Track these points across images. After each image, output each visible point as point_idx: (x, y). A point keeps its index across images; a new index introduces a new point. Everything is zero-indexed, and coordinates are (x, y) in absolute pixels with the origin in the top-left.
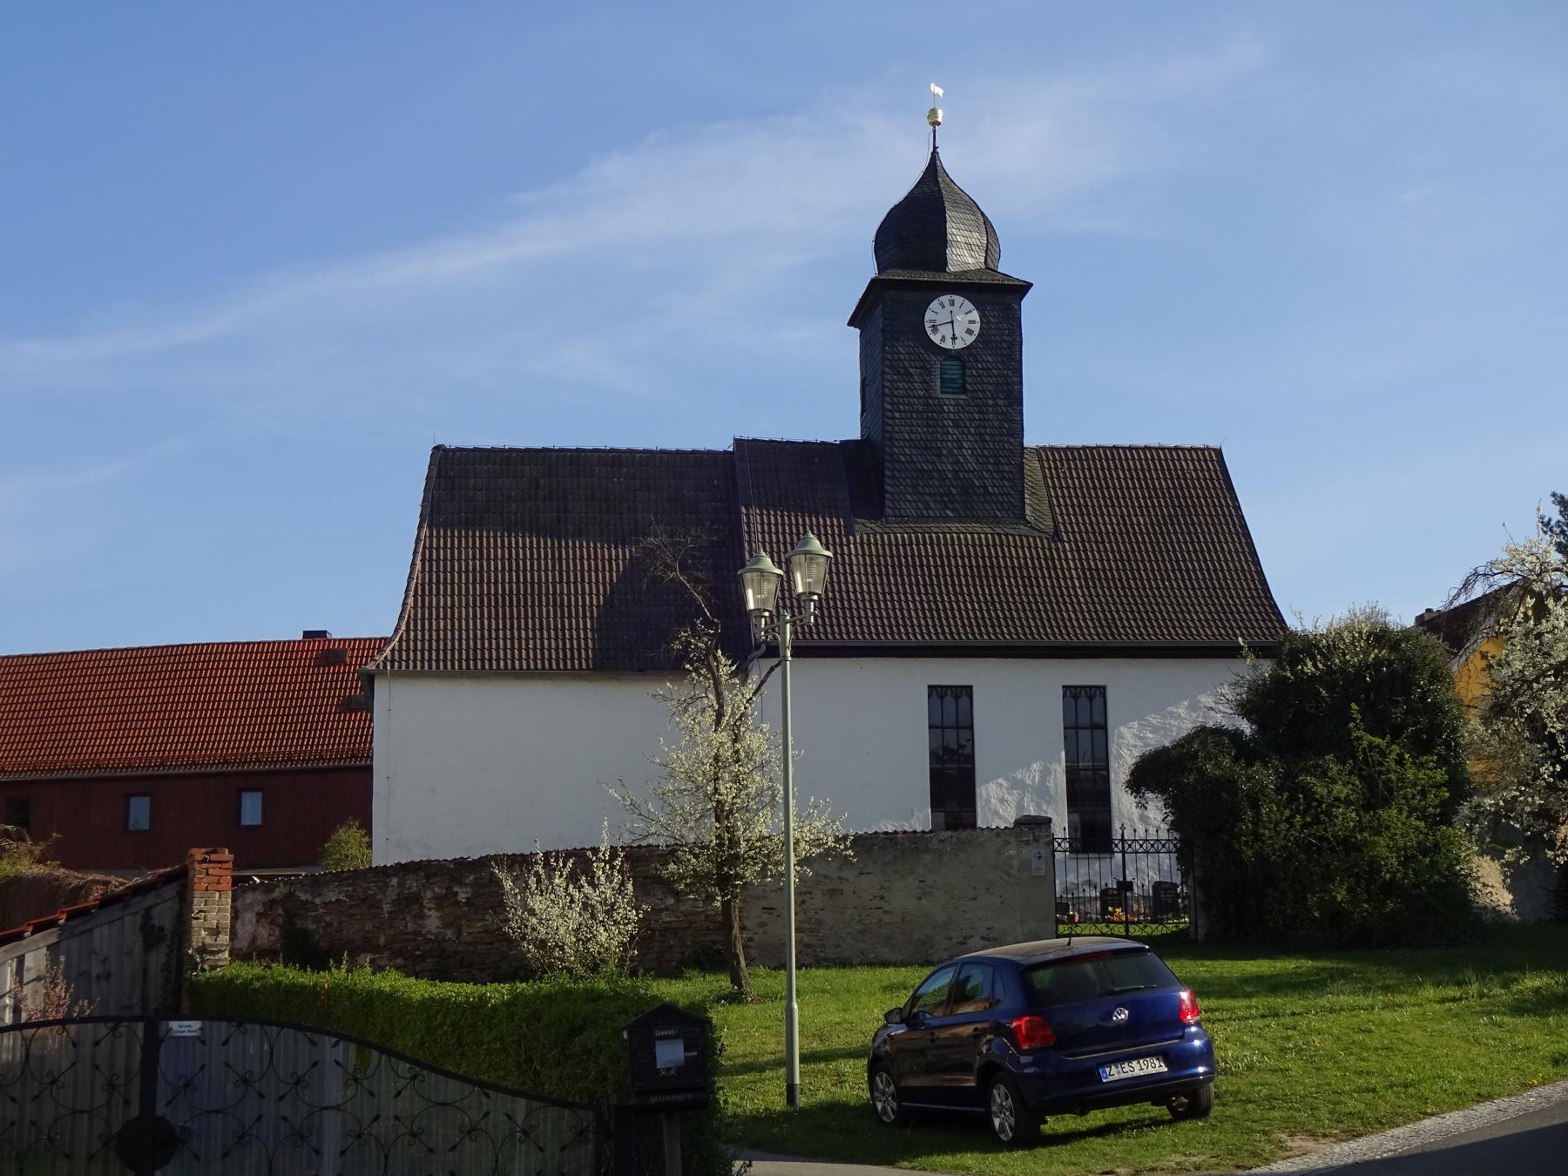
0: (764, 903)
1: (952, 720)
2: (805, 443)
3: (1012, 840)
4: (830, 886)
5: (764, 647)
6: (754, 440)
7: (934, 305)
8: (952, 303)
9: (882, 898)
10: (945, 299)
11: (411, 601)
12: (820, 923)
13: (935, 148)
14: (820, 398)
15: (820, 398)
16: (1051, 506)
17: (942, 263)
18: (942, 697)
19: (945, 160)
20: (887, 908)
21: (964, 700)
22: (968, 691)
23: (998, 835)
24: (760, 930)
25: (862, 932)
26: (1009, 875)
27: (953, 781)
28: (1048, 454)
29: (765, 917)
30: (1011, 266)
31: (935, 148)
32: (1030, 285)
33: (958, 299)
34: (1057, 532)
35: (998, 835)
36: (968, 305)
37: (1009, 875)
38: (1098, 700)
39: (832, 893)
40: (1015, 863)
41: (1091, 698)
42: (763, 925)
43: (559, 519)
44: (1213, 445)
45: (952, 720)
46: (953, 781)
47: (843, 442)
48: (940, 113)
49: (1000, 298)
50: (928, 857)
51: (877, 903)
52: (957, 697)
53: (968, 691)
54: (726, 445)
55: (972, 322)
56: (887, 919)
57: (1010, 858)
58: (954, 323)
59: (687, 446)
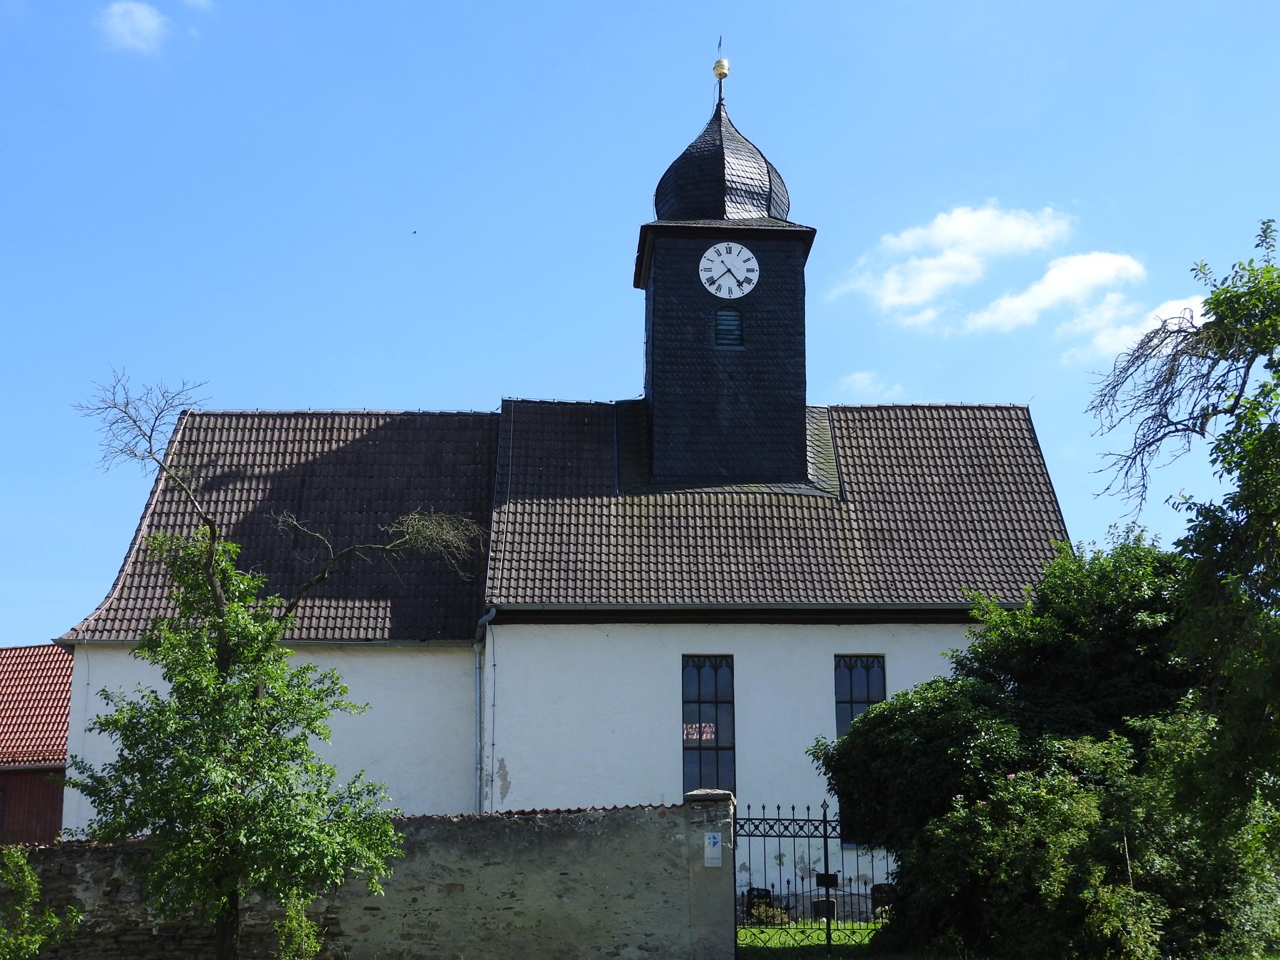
0: (367, 902)
1: (708, 687)
2: (578, 404)
3: (680, 821)
4: (449, 880)
5: (493, 611)
6: (523, 401)
7: (710, 253)
8: (729, 251)
9: (513, 895)
10: (722, 247)
11: (129, 569)
12: (434, 927)
13: (721, 99)
14: (601, 356)
15: (601, 356)
16: (839, 465)
17: (720, 213)
18: (699, 668)
19: (728, 112)
20: (518, 908)
21: (723, 672)
22: (728, 660)
23: (662, 815)
24: (361, 937)
25: (486, 939)
26: (675, 865)
27: (710, 760)
28: (837, 412)
29: (367, 919)
30: (798, 217)
31: (721, 99)
32: (812, 233)
33: (736, 247)
34: (842, 492)
35: (662, 815)
36: (747, 253)
37: (675, 865)
38: (875, 671)
39: (450, 889)
40: (684, 850)
41: (868, 669)
42: (364, 929)
43: (303, 482)
44: (1020, 403)
45: (708, 687)
46: (710, 760)
47: (618, 403)
48: (726, 63)
49: (784, 249)
50: (572, 844)
51: (506, 901)
52: (716, 669)
53: (728, 660)
54: (490, 405)
55: (752, 270)
56: (519, 922)
57: (679, 844)
58: (728, 271)
59: (452, 408)
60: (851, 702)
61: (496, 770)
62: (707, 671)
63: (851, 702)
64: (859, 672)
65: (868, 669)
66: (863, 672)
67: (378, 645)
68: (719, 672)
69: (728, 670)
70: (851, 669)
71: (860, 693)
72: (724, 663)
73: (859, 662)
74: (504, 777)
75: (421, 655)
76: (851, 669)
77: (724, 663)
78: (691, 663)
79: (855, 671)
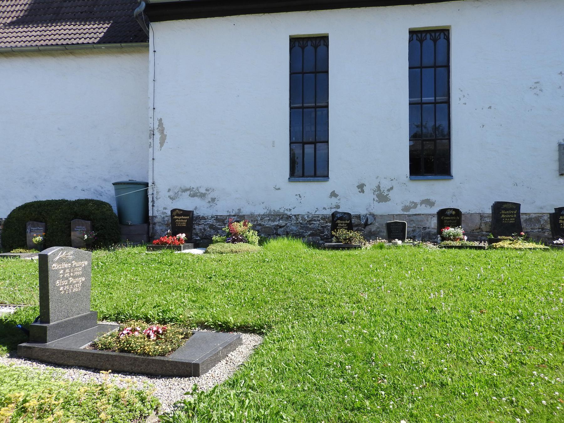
22: (323, 40)
38: (442, 41)
41: (435, 41)
53: (323, 40)
60: (421, 67)
61: (156, 126)
62: (309, 49)
63: (421, 67)
64: (428, 43)
65: (435, 41)
66: (431, 43)
67: (87, 48)
68: (318, 49)
69: (446, 41)
70: (421, 41)
71: (428, 60)
72: (322, 42)
73: (309, 43)
74: (162, 131)
75: (122, 56)
76: (421, 41)
77: (321, 42)
78: (415, 36)
79: (425, 43)
